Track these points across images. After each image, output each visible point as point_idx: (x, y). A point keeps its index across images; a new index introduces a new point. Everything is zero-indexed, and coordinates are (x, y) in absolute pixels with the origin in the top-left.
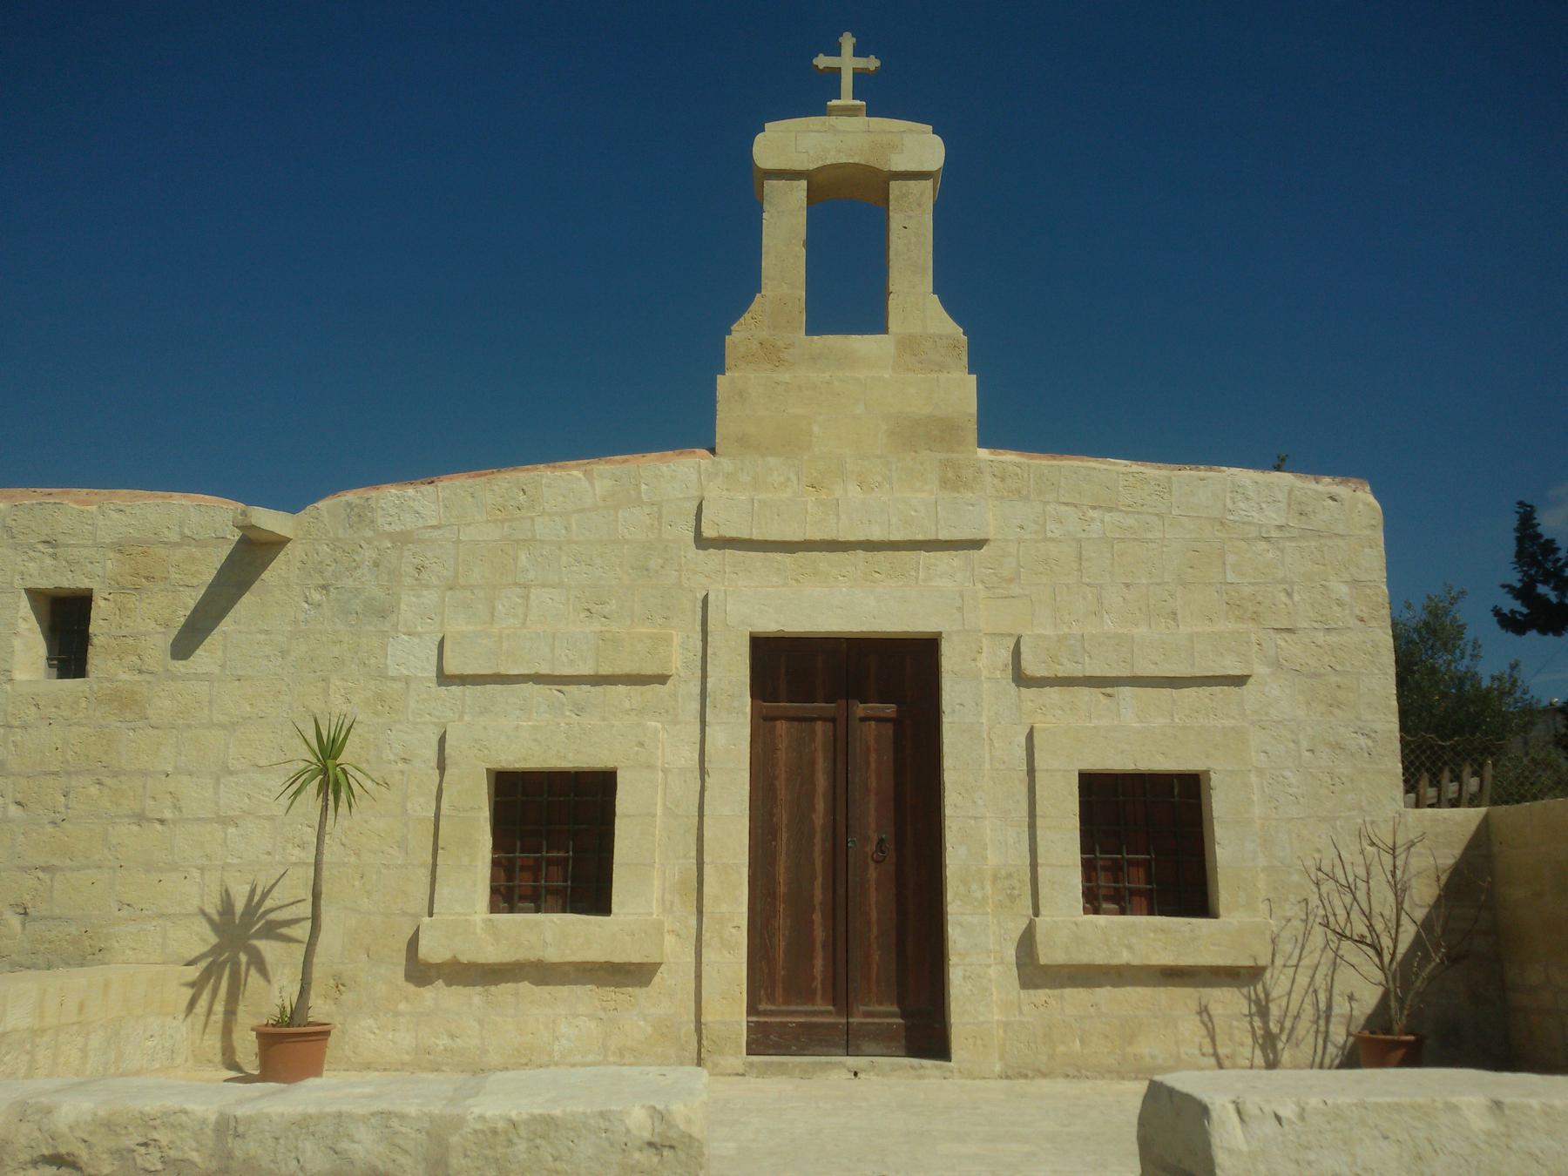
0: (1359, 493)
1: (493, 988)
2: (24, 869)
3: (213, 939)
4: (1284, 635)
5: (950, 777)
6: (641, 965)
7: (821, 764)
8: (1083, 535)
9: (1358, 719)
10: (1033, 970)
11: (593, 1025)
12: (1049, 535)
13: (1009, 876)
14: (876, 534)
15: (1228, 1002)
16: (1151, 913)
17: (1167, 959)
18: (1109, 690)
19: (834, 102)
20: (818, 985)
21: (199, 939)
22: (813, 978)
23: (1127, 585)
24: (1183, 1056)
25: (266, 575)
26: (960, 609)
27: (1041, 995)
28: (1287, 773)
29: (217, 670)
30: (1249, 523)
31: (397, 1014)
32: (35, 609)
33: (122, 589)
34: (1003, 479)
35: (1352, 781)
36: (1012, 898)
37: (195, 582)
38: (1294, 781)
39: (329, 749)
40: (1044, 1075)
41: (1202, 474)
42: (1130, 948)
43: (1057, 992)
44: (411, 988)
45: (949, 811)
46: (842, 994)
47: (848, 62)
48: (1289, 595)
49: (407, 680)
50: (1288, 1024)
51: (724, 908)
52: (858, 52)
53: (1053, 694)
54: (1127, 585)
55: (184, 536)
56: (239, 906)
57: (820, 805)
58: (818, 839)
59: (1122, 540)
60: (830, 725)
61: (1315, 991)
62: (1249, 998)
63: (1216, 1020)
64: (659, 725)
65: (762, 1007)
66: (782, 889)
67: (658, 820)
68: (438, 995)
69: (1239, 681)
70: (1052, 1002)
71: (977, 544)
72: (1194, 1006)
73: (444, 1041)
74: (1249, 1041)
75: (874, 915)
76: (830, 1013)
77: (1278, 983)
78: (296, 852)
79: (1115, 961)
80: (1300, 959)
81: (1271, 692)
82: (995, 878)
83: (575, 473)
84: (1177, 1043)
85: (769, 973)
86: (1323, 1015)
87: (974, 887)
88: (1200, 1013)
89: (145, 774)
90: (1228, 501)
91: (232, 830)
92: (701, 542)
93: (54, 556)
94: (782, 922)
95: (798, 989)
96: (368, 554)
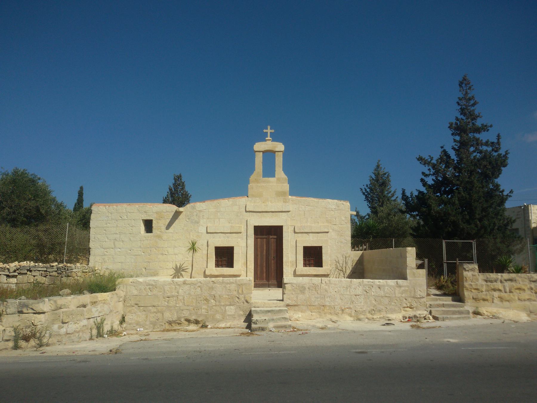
5: (284, 247)
10: (295, 275)
33: (157, 219)
39: (193, 244)
46: (268, 279)
47: (269, 131)
49: (202, 233)
53: (300, 235)
56: (178, 267)
57: (265, 251)
69: (327, 232)
71: (289, 212)
81: (332, 234)
96: (195, 214)
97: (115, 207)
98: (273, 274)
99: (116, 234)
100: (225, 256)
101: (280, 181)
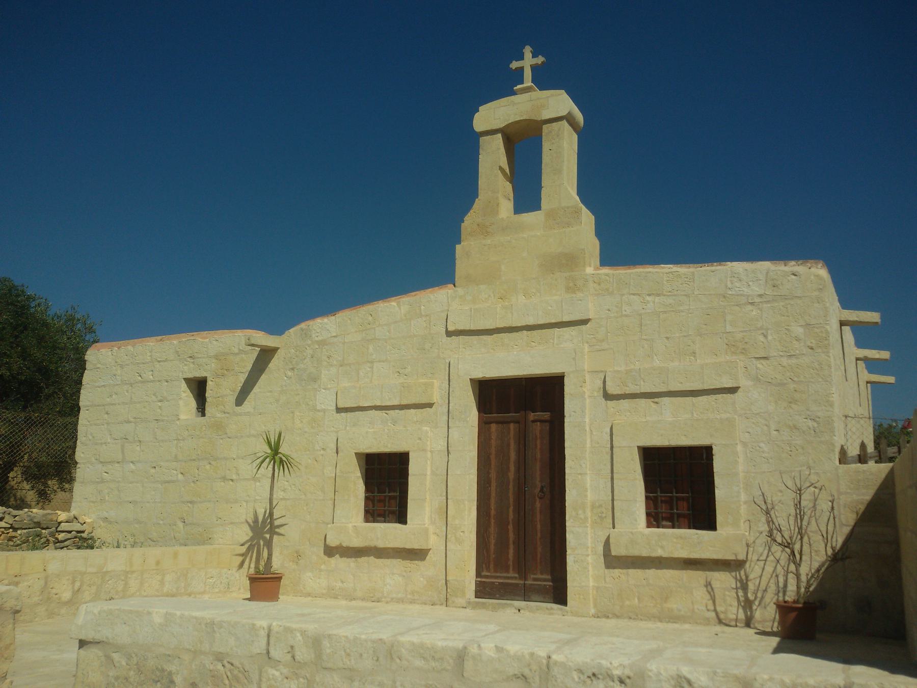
0: (812, 269)
1: (359, 559)
2: (183, 502)
3: (251, 534)
4: (762, 361)
5: (568, 452)
6: (421, 550)
7: (513, 445)
8: (643, 311)
9: (808, 410)
10: (612, 561)
11: (400, 579)
12: (624, 313)
13: (600, 506)
14: (531, 321)
15: (723, 580)
16: (690, 528)
17: (684, 554)
18: (656, 400)
19: (519, 87)
20: (511, 563)
21: (244, 533)
22: (508, 559)
23: (667, 338)
24: (696, 611)
25: (270, 365)
26: (574, 359)
27: (617, 572)
28: (762, 445)
29: (252, 410)
30: (741, 295)
31: (321, 570)
32: (189, 387)
33: (217, 376)
34: (599, 284)
35: (803, 448)
36: (601, 518)
37: (244, 370)
38: (766, 449)
39: (275, 450)
40: (618, 617)
41: (713, 268)
42: (662, 547)
43: (625, 571)
44: (326, 558)
45: (567, 471)
46: (522, 569)
47: (528, 61)
48: (765, 336)
49: (324, 411)
50: (759, 595)
51: (457, 522)
52: (521, 57)
53: (625, 403)
54: (667, 338)
55: (240, 350)
56: (260, 518)
57: (512, 468)
58: (511, 487)
59: (665, 312)
60: (517, 425)
61: (777, 576)
62: (736, 578)
63: (716, 590)
64: (428, 429)
65: (485, 573)
66: (493, 512)
67: (428, 478)
68: (337, 561)
69: (733, 390)
70: (622, 576)
71: (585, 322)
72: (703, 582)
73: (339, 584)
74: (736, 604)
75: (539, 526)
76: (516, 578)
77: (754, 571)
78: (282, 493)
79: (654, 555)
80: (767, 556)
81: (753, 396)
82: (593, 507)
83: (393, 303)
84: (692, 603)
85: (487, 556)
86: (781, 591)
87: (580, 512)
88: (706, 586)
89: (225, 459)
90: (729, 283)
91: (258, 484)
92: (449, 334)
93: (193, 363)
94: (493, 529)
95: (501, 565)
96: (309, 351)
97: (130, 348)
98: (539, 549)
99: (128, 422)
100: (386, 482)
101: (567, 215)
